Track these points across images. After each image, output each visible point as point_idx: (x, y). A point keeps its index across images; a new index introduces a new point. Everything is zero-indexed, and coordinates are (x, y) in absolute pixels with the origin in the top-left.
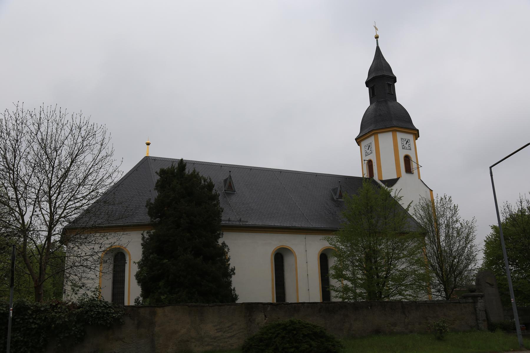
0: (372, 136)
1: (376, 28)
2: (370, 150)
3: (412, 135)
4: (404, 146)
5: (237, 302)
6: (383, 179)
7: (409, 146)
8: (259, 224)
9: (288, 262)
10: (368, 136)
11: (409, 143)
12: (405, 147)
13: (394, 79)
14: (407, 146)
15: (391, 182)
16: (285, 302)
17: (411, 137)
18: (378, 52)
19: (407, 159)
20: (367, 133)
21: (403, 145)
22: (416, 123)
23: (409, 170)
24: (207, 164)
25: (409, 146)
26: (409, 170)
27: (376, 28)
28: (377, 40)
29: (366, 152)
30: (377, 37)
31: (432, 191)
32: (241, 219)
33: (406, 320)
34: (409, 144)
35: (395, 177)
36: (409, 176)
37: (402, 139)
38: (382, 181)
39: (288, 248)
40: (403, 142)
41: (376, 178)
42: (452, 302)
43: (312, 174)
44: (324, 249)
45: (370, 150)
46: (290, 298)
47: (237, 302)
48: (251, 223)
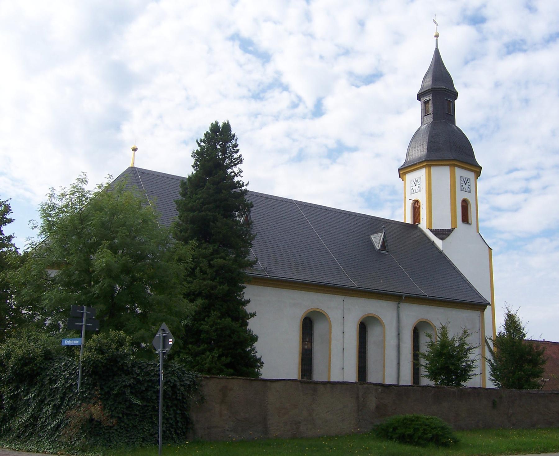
0: (424, 168)
1: (436, 23)
2: (419, 187)
3: (474, 173)
4: (463, 187)
5: (467, 384)
6: (433, 228)
7: (468, 187)
8: (324, 282)
9: (318, 329)
10: (418, 168)
11: (469, 184)
12: (464, 188)
13: (454, 94)
14: (466, 187)
15: (443, 234)
16: (365, 381)
17: (471, 175)
19: (465, 205)
20: (416, 164)
21: (462, 186)
22: (480, 159)
23: (465, 219)
24: (320, 207)
25: (468, 187)
26: (465, 219)
27: (436, 23)
28: (437, 40)
29: (412, 189)
31: (491, 249)
32: (267, 268)
33: (509, 411)
34: (469, 185)
35: (449, 227)
36: (465, 226)
37: (461, 177)
38: (435, 232)
39: (428, 322)
40: (462, 182)
41: (423, 225)
42: (554, 393)
43: (335, 210)
44: (311, 311)
45: (419, 187)
46: (373, 377)
47: (467, 384)
48: (279, 274)
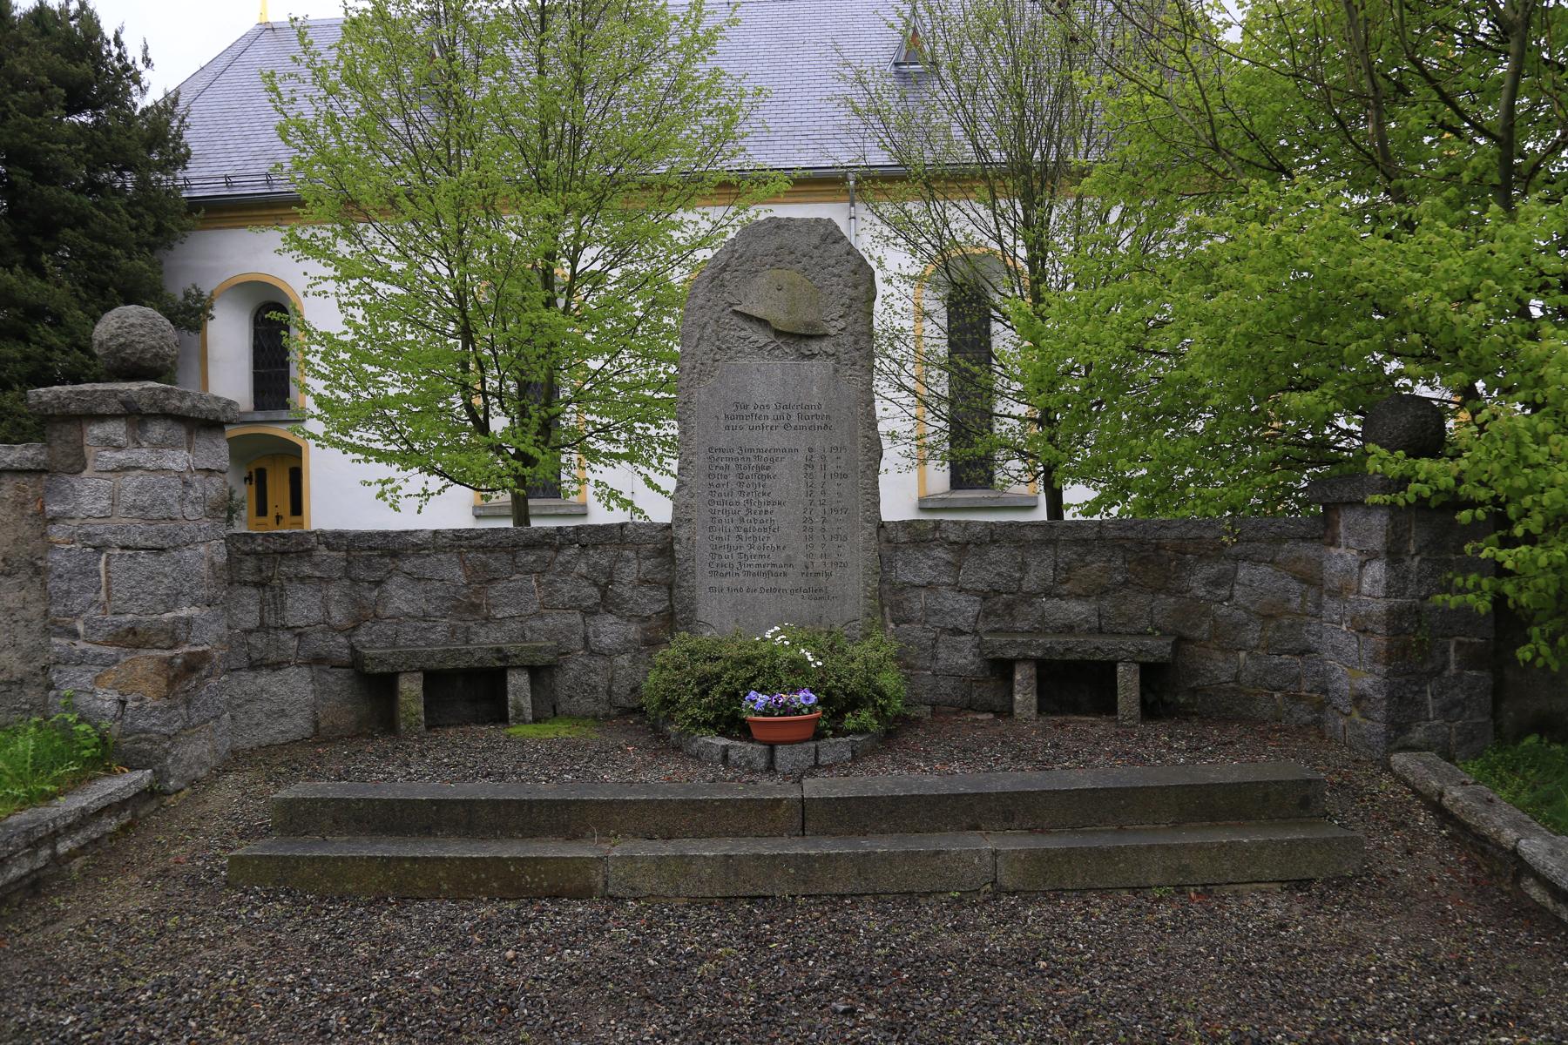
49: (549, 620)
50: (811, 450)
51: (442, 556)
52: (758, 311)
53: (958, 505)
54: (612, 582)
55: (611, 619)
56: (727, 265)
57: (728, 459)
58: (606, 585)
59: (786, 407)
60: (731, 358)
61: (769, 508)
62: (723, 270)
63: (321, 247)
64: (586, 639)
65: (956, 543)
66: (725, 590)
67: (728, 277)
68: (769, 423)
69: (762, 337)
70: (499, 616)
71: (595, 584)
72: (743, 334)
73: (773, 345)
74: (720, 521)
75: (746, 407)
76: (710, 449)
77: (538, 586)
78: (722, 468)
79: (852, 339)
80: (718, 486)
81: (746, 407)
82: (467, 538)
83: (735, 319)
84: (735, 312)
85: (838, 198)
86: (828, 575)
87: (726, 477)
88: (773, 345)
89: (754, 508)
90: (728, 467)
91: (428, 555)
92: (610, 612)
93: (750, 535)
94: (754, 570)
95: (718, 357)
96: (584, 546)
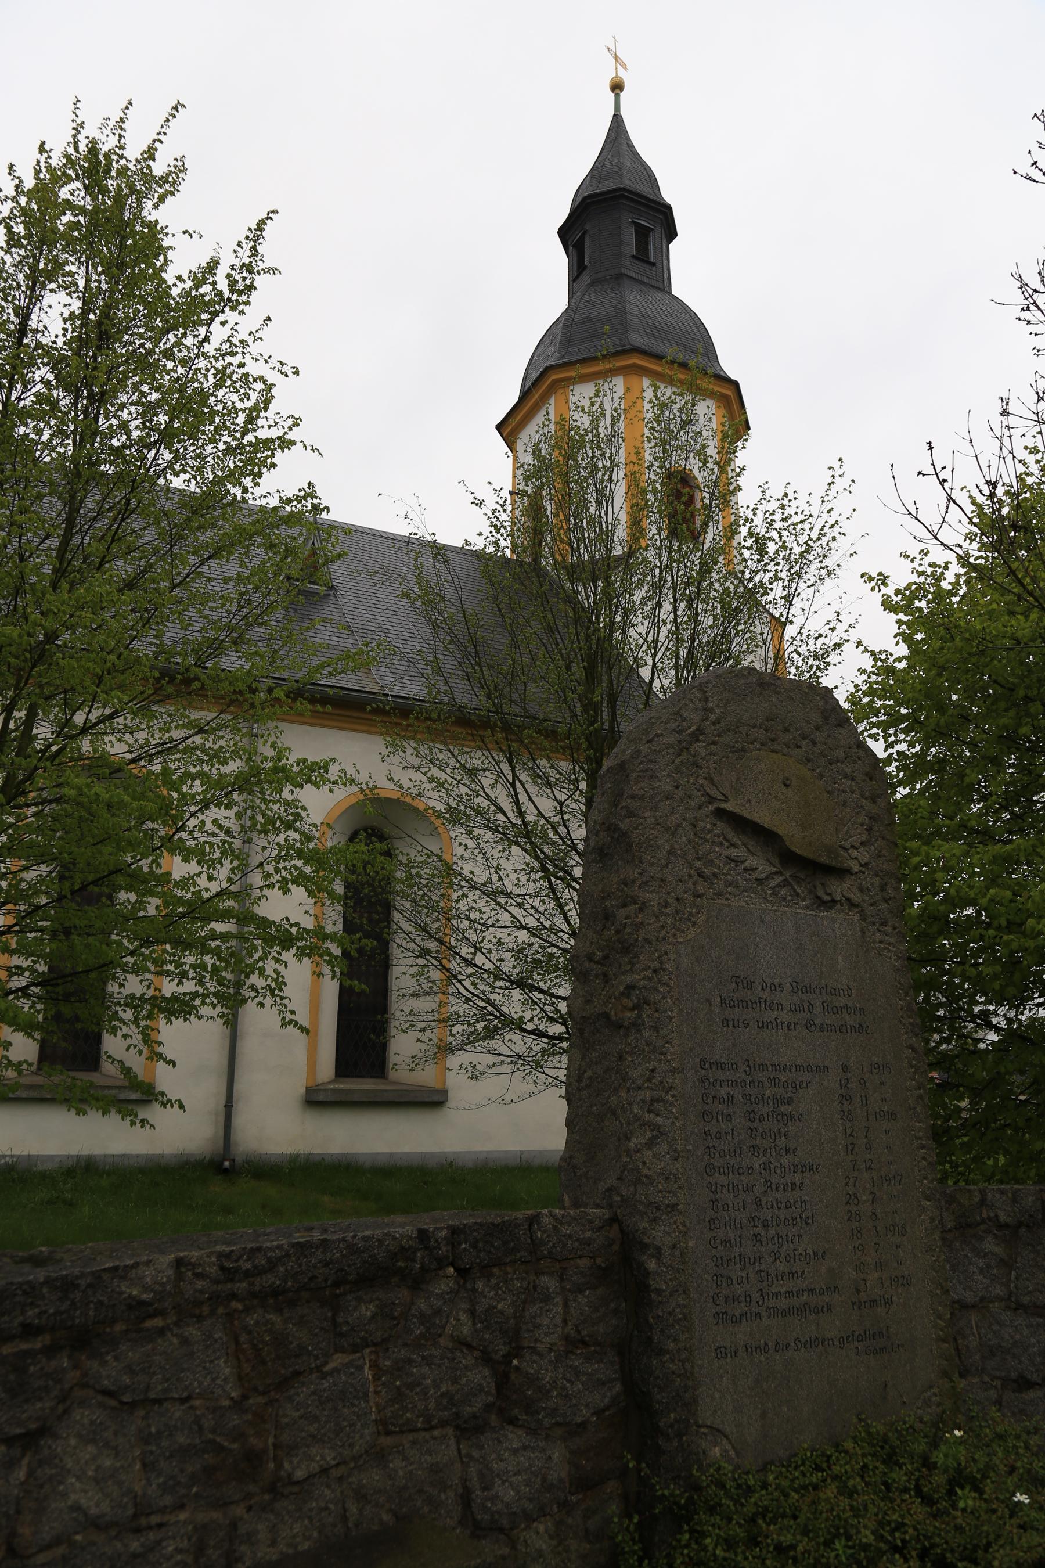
18: (617, 124)
30: (617, 87)
49: (396, 1463)
50: (845, 1068)
51: (192, 1331)
52: (762, 817)
53: (356, 1098)
54: (517, 1351)
55: (514, 1438)
56: (700, 731)
57: (734, 1083)
58: (508, 1357)
59: (807, 989)
60: (719, 894)
61: (797, 1179)
62: (695, 737)
63: (145, 388)
64: (466, 1498)
65: (1006, 1226)
66: (741, 1352)
67: (703, 752)
68: (785, 1016)
69: (761, 863)
70: (300, 1474)
71: (486, 1359)
72: (734, 853)
73: (778, 879)
74: (725, 1207)
75: (750, 986)
76: (703, 1061)
77: (376, 1378)
78: (721, 1101)
79: (877, 881)
80: (719, 1136)
81: (750, 986)
82: (247, 1274)
83: (721, 827)
84: (720, 813)
85: (373, 729)
86: (888, 1302)
87: (729, 1118)
88: (778, 879)
89: (775, 1179)
90: (731, 1098)
91: (161, 1332)
92: (513, 1422)
93: (772, 1232)
94: (782, 1303)
95: (700, 889)
96: (463, 1273)
